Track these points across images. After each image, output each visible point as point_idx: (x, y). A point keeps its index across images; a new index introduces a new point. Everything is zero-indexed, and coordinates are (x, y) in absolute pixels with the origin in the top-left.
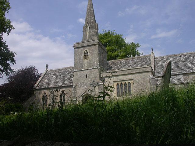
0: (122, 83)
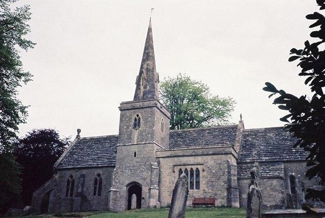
0: (192, 169)
